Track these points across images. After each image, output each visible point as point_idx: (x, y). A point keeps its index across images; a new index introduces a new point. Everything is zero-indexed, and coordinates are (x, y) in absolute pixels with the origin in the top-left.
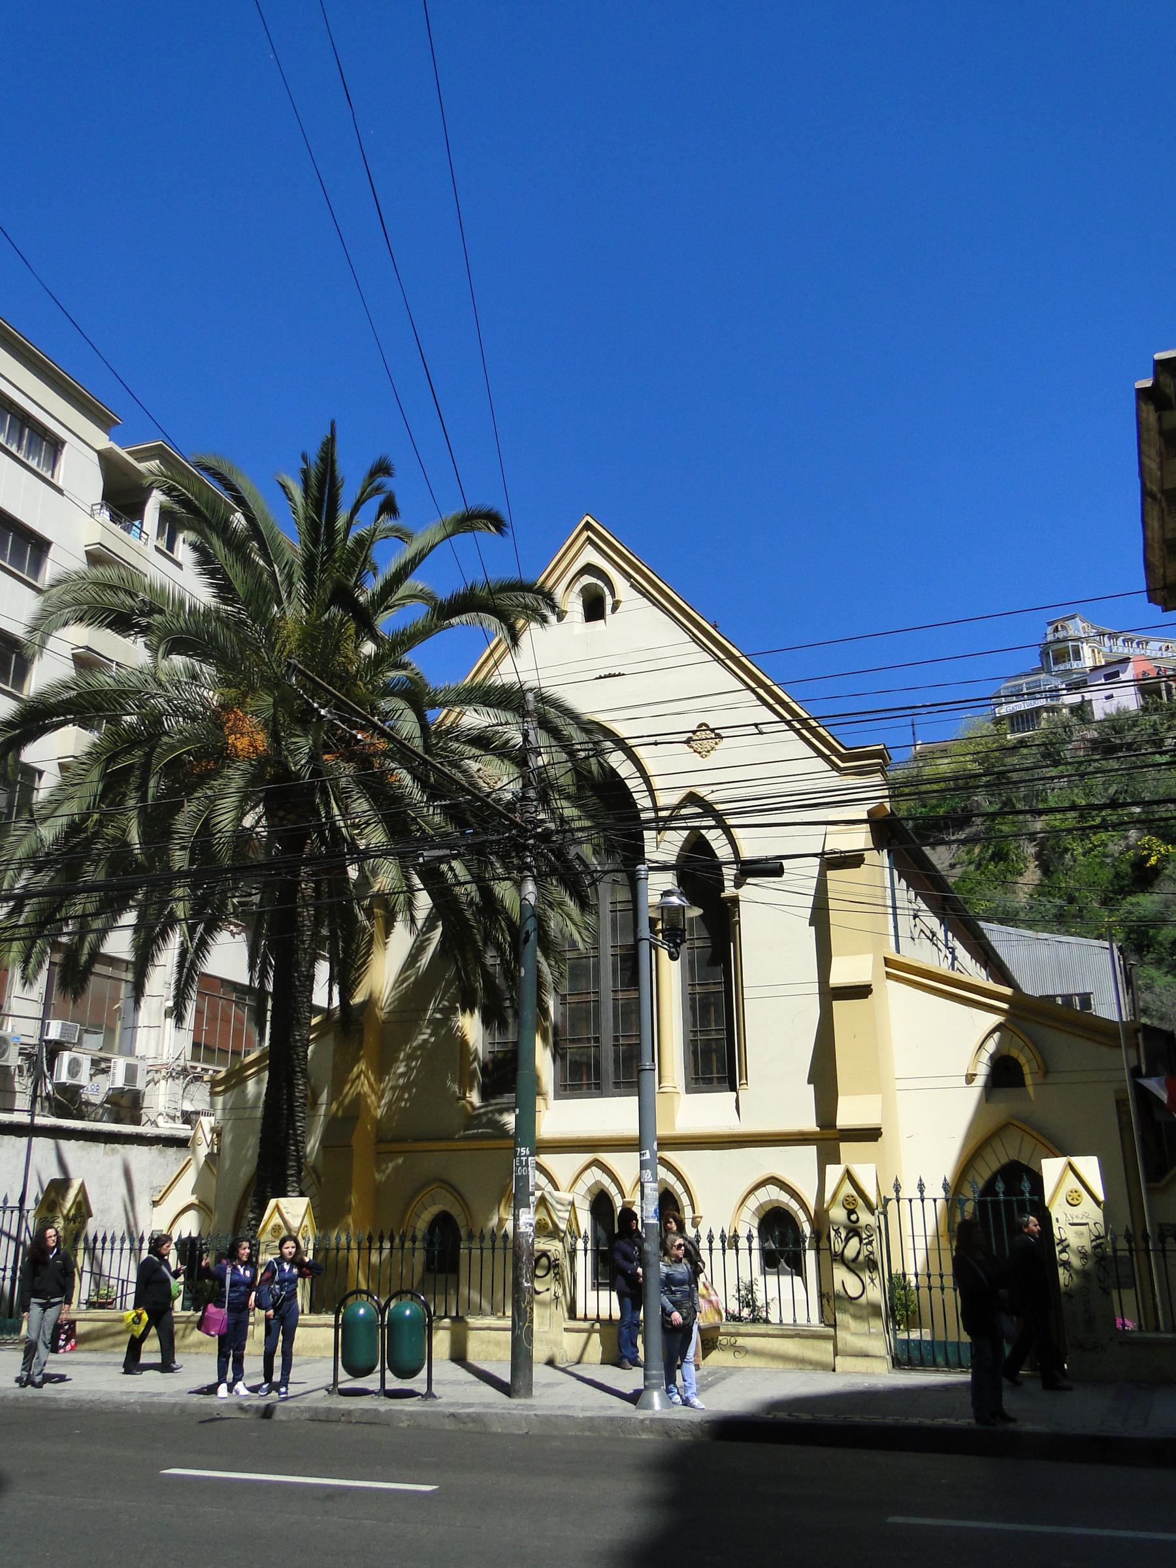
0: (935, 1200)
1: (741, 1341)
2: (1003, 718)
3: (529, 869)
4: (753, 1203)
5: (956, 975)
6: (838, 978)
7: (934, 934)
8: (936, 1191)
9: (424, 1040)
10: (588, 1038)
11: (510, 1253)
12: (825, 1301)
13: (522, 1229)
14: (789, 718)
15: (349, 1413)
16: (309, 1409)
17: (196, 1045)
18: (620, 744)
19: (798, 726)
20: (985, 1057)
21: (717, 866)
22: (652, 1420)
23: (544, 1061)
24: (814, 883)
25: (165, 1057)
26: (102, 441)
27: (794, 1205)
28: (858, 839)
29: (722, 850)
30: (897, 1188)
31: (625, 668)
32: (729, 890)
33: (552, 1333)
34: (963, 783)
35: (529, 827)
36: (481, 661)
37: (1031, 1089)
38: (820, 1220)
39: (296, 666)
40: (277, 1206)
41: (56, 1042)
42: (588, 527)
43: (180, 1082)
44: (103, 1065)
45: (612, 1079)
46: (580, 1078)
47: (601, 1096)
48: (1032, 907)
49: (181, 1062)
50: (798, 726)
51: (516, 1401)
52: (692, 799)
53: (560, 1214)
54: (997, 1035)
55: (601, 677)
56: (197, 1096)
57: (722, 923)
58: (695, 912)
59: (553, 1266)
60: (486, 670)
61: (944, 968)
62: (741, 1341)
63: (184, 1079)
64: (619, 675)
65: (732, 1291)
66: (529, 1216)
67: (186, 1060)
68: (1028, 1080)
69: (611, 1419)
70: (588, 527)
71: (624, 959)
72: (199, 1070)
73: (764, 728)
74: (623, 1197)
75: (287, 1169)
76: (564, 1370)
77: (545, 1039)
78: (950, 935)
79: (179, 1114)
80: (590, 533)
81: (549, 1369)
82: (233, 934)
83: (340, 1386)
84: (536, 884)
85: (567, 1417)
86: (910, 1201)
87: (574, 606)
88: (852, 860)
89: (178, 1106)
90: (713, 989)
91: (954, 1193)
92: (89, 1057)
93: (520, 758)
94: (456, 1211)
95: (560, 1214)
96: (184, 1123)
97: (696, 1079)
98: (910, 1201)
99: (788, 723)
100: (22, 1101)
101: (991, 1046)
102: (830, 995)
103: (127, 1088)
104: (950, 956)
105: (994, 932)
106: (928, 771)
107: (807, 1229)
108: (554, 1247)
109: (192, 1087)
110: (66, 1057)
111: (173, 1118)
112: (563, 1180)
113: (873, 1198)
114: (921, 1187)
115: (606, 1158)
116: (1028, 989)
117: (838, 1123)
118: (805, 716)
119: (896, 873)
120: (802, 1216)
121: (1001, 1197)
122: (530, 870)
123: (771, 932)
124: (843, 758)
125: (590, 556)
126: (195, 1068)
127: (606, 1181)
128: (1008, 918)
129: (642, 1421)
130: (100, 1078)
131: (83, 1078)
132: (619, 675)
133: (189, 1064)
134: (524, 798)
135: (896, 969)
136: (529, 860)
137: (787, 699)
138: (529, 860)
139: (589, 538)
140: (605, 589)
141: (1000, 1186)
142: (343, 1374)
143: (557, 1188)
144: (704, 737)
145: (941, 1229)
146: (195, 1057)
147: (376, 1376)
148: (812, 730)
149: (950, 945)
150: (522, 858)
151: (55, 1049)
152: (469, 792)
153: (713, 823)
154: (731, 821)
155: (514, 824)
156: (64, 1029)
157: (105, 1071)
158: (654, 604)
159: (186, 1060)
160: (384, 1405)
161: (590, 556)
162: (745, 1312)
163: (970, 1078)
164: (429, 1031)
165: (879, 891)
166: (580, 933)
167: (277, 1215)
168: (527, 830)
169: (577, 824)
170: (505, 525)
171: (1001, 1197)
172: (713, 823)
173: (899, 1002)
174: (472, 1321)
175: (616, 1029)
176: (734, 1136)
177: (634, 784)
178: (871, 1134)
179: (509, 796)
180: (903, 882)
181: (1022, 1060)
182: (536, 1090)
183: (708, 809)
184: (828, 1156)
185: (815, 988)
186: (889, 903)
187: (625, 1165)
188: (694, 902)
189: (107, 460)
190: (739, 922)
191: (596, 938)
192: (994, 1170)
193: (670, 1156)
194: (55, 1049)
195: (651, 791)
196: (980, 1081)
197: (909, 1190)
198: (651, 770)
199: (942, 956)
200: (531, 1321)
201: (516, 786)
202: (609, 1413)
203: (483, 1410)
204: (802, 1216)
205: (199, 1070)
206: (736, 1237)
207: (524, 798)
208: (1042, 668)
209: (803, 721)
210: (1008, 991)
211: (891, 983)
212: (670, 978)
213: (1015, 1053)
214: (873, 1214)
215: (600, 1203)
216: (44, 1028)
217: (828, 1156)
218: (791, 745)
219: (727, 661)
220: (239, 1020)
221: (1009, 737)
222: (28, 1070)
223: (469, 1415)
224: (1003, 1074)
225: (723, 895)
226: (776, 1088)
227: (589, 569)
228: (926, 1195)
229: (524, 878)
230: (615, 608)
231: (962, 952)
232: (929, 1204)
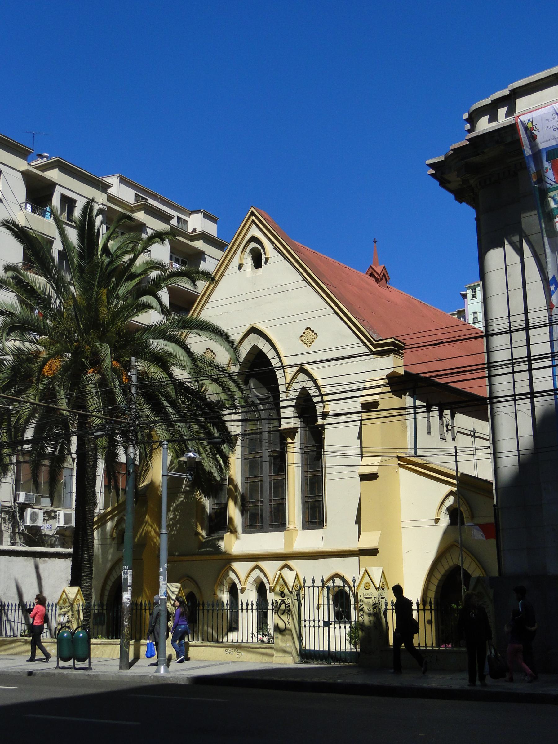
0: (318, 587)
9: (181, 501)
23: (234, 512)
26: (23, 165)
31: (263, 301)
41: (23, 504)
44: (53, 514)
45: (268, 523)
46: (254, 523)
70: (253, 214)
71: (275, 458)
75: (82, 573)
77: (236, 503)
80: (253, 218)
85: (126, 675)
86: (309, 587)
92: (42, 511)
94: (195, 591)
98: (309, 587)
100: (7, 537)
103: (66, 526)
110: (29, 511)
112: (243, 577)
114: (313, 581)
115: (262, 564)
124: (375, 346)
125: (255, 232)
127: (262, 576)
130: (51, 522)
131: (40, 522)
136: (131, 437)
138: (131, 437)
139: (253, 221)
140: (262, 251)
151: (23, 507)
156: (27, 497)
157: (54, 518)
161: (255, 232)
164: (183, 496)
175: (271, 496)
176: (319, 553)
189: (26, 175)
194: (23, 507)
197: (309, 583)
211: (401, 470)
216: (16, 497)
222: (9, 520)
223: (94, 675)
227: (253, 239)
230: (266, 262)
232: (316, 588)
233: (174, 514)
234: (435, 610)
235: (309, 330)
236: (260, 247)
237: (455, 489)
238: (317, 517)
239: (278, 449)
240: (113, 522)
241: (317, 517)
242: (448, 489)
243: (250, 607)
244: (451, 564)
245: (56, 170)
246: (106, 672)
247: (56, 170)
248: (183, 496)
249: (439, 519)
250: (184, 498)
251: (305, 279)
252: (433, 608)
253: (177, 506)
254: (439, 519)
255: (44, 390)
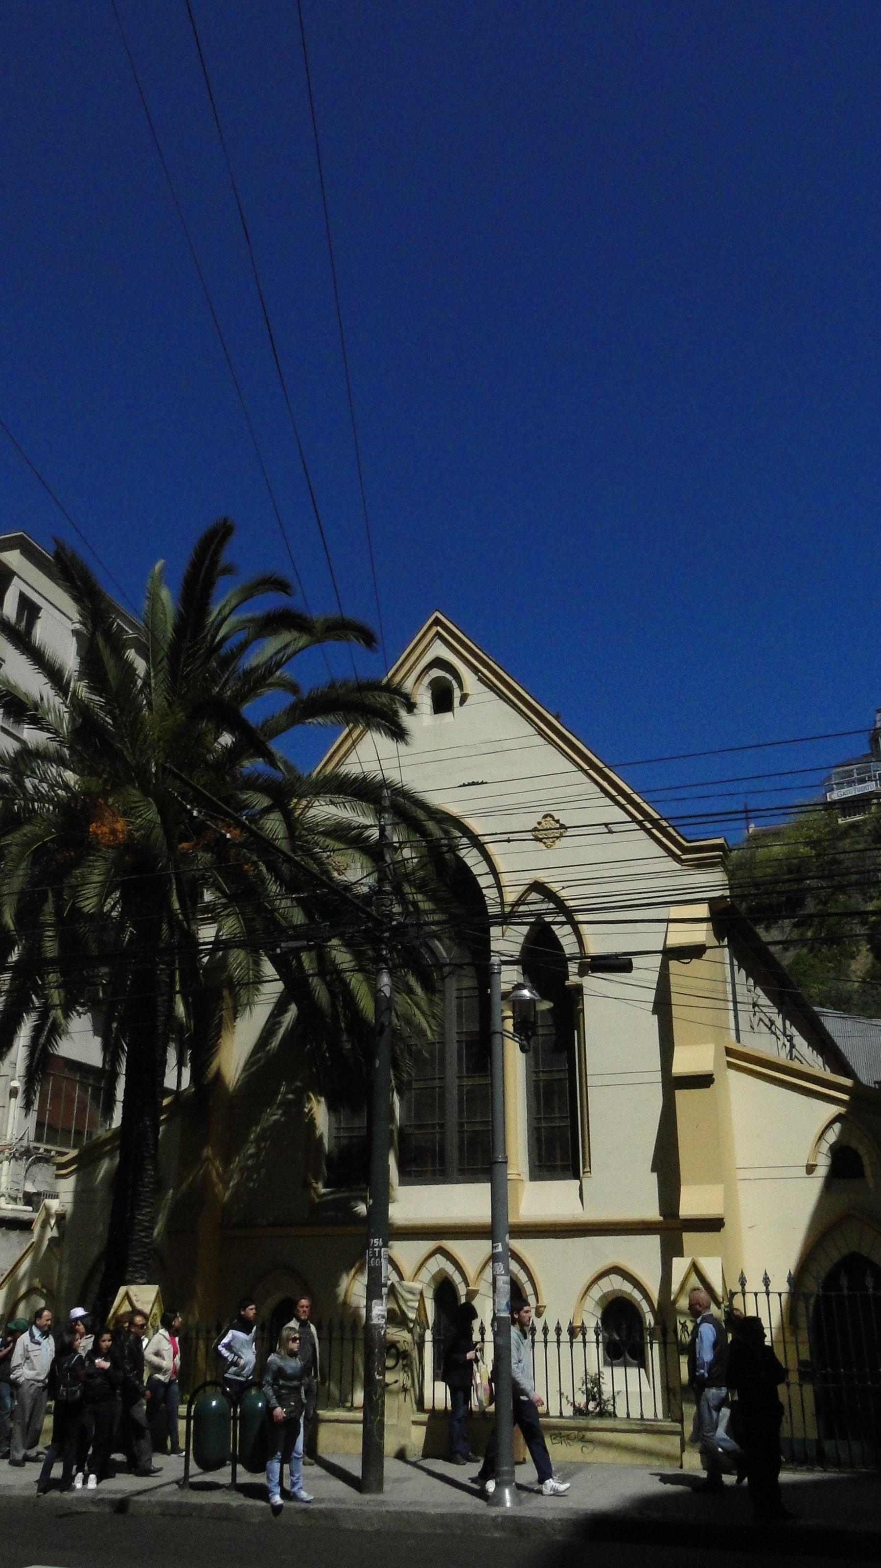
0: (780, 1294)
1: (589, 1435)
2: (834, 803)
3: (385, 960)
4: (596, 1293)
5: (795, 1065)
6: (682, 1065)
7: (772, 1023)
8: (780, 1285)
10: (433, 1124)
11: (361, 1346)
12: (671, 1397)
13: (375, 1321)
14: (641, 818)
15: (200, 1508)
16: (159, 1503)
17: (40, 1125)
18: (476, 842)
19: (649, 826)
20: (825, 1147)
21: (564, 961)
22: (505, 1518)
24: (655, 976)
25: (8, 1137)
27: (637, 1295)
28: (700, 934)
29: (569, 945)
30: (743, 1281)
32: (573, 979)
33: (405, 1429)
34: (796, 869)
35: (385, 920)
36: (332, 750)
37: (871, 1181)
38: (665, 1309)
39: (171, 770)
40: (127, 1295)
42: (437, 622)
43: (23, 1163)
46: (425, 1167)
47: (444, 1183)
48: (864, 991)
49: (25, 1143)
50: (649, 826)
51: (368, 1497)
52: (537, 887)
53: (410, 1304)
54: (837, 1127)
55: (464, 785)
56: (39, 1178)
57: (568, 1010)
58: (545, 1006)
59: (403, 1356)
60: (336, 759)
61: (782, 1058)
62: (589, 1435)
63: (27, 1159)
64: (482, 783)
65: (578, 1384)
66: (380, 1308)
67: (29, 1140)
68: (868, 1171)
69: (463, 1517)
70: (437, 622)
72: (41, 1150)
73: (614, 828)
74: (467, 1285)
76: (415, 1464)
78: (788, 1023)
79: (21, 1195)
80: (439, 628)
81: (400, 1464)
82: (79, 1014)
83: (191, 1480)
84: (391, 976)
85: (419, 1513)
86: (756, 1294)
87: (424, 699)
88: (695, 952)
89: (20, 1187)
90: (557, 1076)
91: (796, 1281)
93: (375, 852)
95: (410, 1304)
96: (25, 1204)
97: (540, 1166)
98: (756, 1294)
99: (639, 823)
101: (832, 1137)
102: (673, 1084)
104: (788, 1044)
105: (834, 1024)
106: (761, 854)
107: (649, 1319)
108: (401, 1336)
109: (35, 1169)
111: (15, 1200)
112: (408, 1269)
113: (719, 1290)
114: (766, 1281)
115: (451, 1245)
116: (866, 1078)
117: (681, 1213)
118: (656, 816)
119: (736, 963)
120: (645, 1307)
121: (846, 1292)
122: (386, 963)
123: (614, 1024)
125: (439, 650)
126: (38, 1149)
127: (450, 1269)
128: (843, 1004)
129: (494, 1519)
132: (482, 783)
133: (32, 1145)
134: (380, 892)
135: (739, 1059)
137: (629, 791)
138: (384, 952)
139: (438, 633)
140: (454, 683)
141: (844, 1281)
142: (194, 1468)
143: (402, 1278)
144: (548, 832)
145: (784, 1319)
146: (38, 1138)
147: (228, 1469)
148: (662, 830)
149: (788, 1033)
150: (377, 951)
152: (323, 884)
153: (563, 919)
154: (580, 917)
155: (370, 916)
158: (501, 698)
159: (29, 1140)
160: (236, 1500)
161: (439, 650)
162: (592, 1406)
163: (810, 1169)
164: (280, 1112)
165: (720, 986)
166: (428, 1022)
167: (127, 1303)
168: (382, 923)
169: (430, 918)
170: (374, 641)
171: (846, 1292)
172: (563, 919)
173: (741, 1091)
174: (323, 1413)
175: (460, 1116)
177: (485, 881)
178: (714, 1225)
179: (365, 889)
180: (743, 972)
181: (862, 1151)
182: (387, 1184)
183: (561, 906)
184: (671, 1249)
185: (658, 1077)
186: (730, 998)
187: (471, 1254)
188: (544, 996)
190: (582, 1010)
191: (442, 1026)
192: (835, 1261)
193: (517, 1245)
195: (499, 886)
196: (822, 1171)
197: (754, 1284)
198: (501, 866)
199: (780, 1044)
200: (383, 1415)
201: (371, 880)
202: (461, 1509)
203: (334, 1505)
204: (645, 1307)
205: (41, 1150)
206: (583, 1329)
207: (380, 892)
208: (872, 754)
209: (655, 822)
210: (848, 1082)
211: (732, 1073)
212: (515, 1064)
213: (854, 1144)
214: (719, 1308)
215: (444, 1289)
217: (671, 1249)
218: (640, 845)
219: (591, 772)
220: (82, 1102)
221: (840, 821)
223: (320, 1511)
224: (844, 1165)
225: (567, 983)
226: (618, 1177)
227: (438, 663)
228: (771, 1289)
229: (379, 972)
231: (800, 1042)
232: (774, 1298)
233: (258, 1147)
234: (603, 1342)
235: (549, 819)
236: (448, 676)
237: (842, 1110)
238: (558, 1157)
239: (476, 1028)
240: (112, 1159)
241: (558, 1157)
242: (834, 1110)
243: (552, 1336)
244: (845, 1251)
245: (17, 552)
246: (415, 1503)
247: (17, 552)
248: (280, 1112)
249: (816, 1165)
250: (282, 1115)
251: (541, 733)
252: (600, 1338)
253: (264, 1130)
254: (816, 1165)
255: (110, 870)
